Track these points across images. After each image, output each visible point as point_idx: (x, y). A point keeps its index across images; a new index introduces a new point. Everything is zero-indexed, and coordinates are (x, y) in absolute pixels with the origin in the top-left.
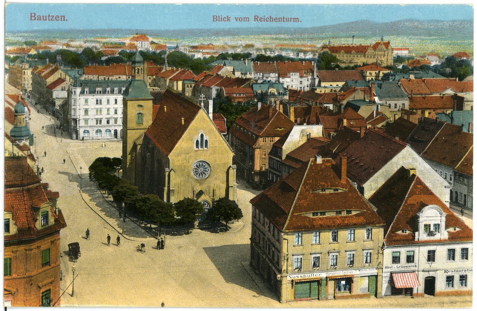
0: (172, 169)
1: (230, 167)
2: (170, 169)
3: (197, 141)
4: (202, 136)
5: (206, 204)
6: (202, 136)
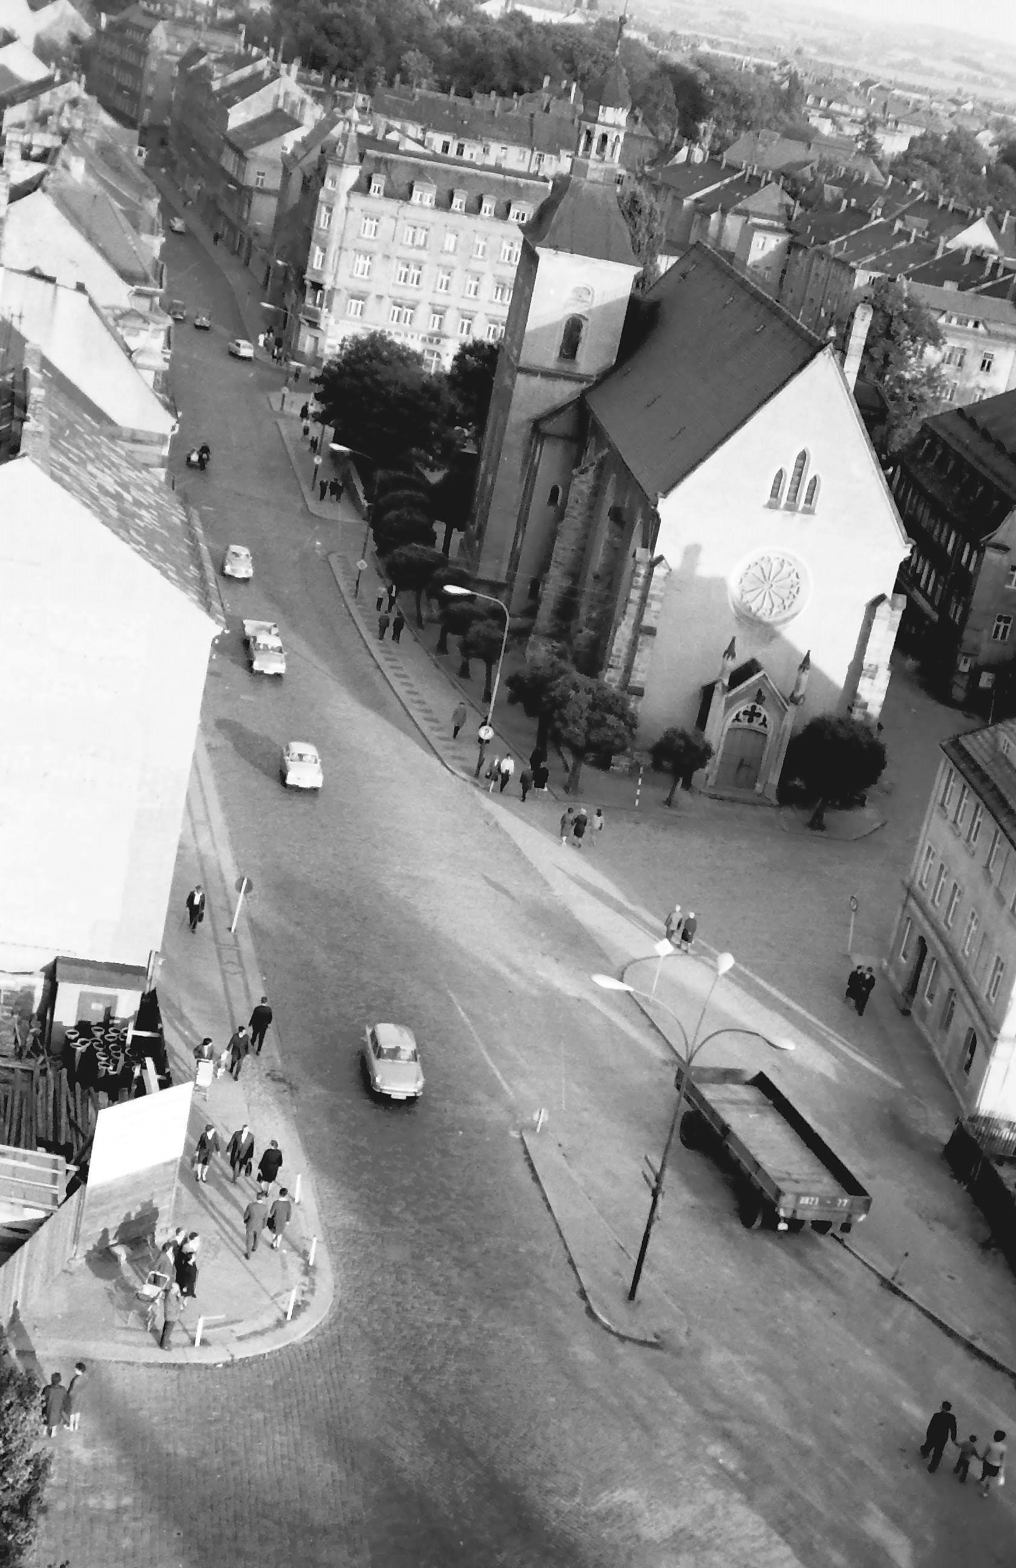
0: (661, 558)
1: (881, 598)
2: (656, 554)
3: (780, 474)
4: (803, 456)
5: (759, 715)
6: (803, 456)
